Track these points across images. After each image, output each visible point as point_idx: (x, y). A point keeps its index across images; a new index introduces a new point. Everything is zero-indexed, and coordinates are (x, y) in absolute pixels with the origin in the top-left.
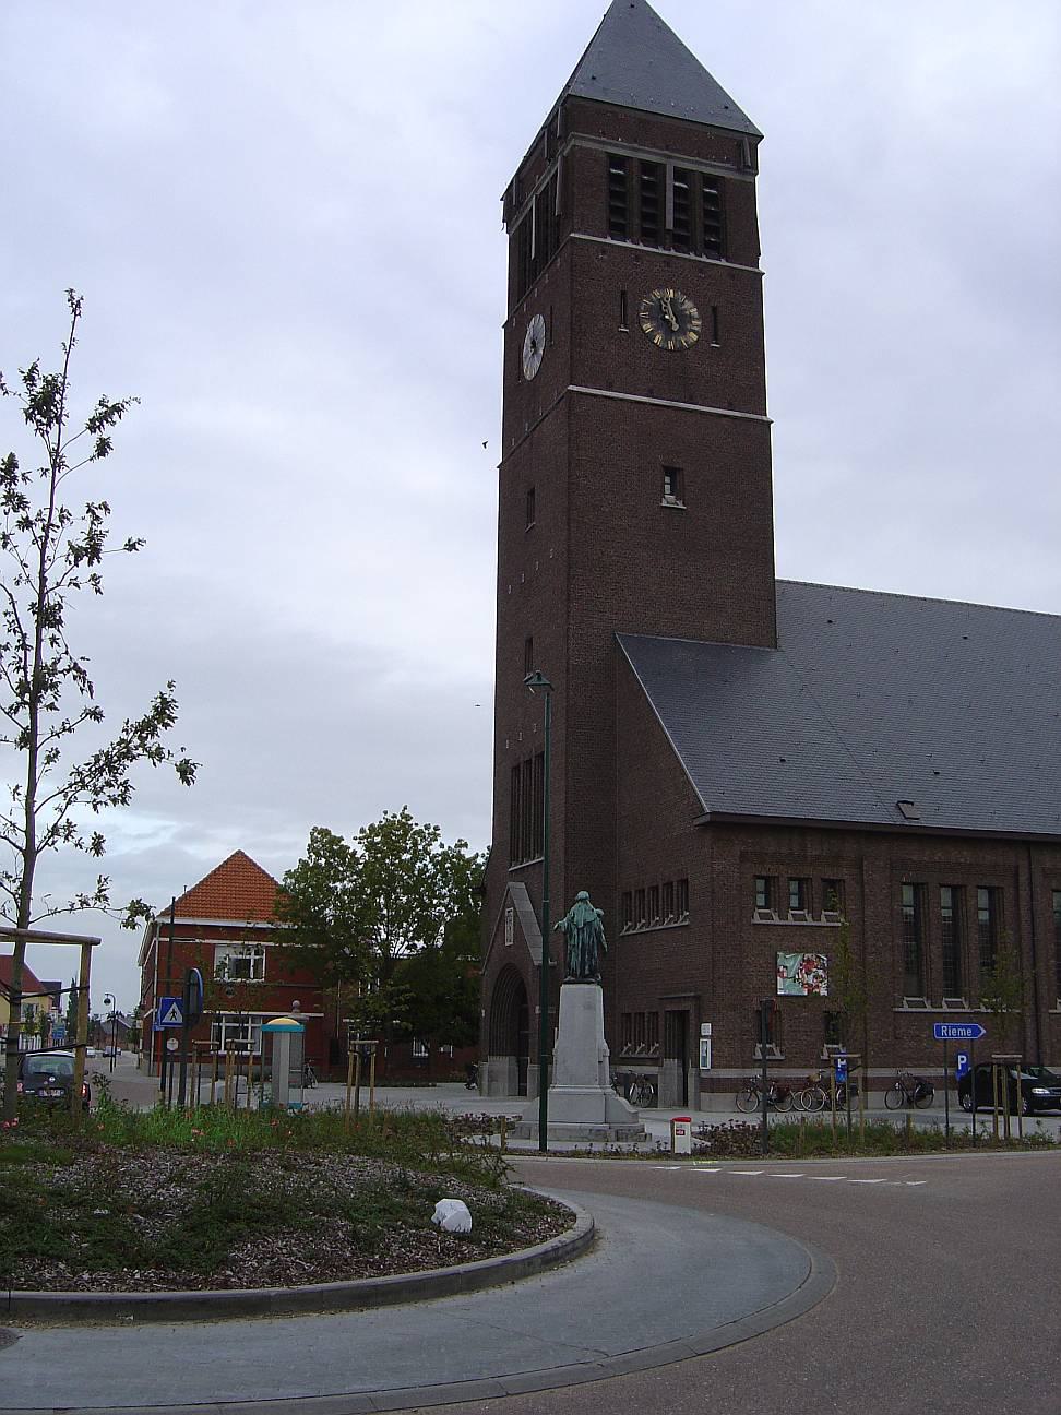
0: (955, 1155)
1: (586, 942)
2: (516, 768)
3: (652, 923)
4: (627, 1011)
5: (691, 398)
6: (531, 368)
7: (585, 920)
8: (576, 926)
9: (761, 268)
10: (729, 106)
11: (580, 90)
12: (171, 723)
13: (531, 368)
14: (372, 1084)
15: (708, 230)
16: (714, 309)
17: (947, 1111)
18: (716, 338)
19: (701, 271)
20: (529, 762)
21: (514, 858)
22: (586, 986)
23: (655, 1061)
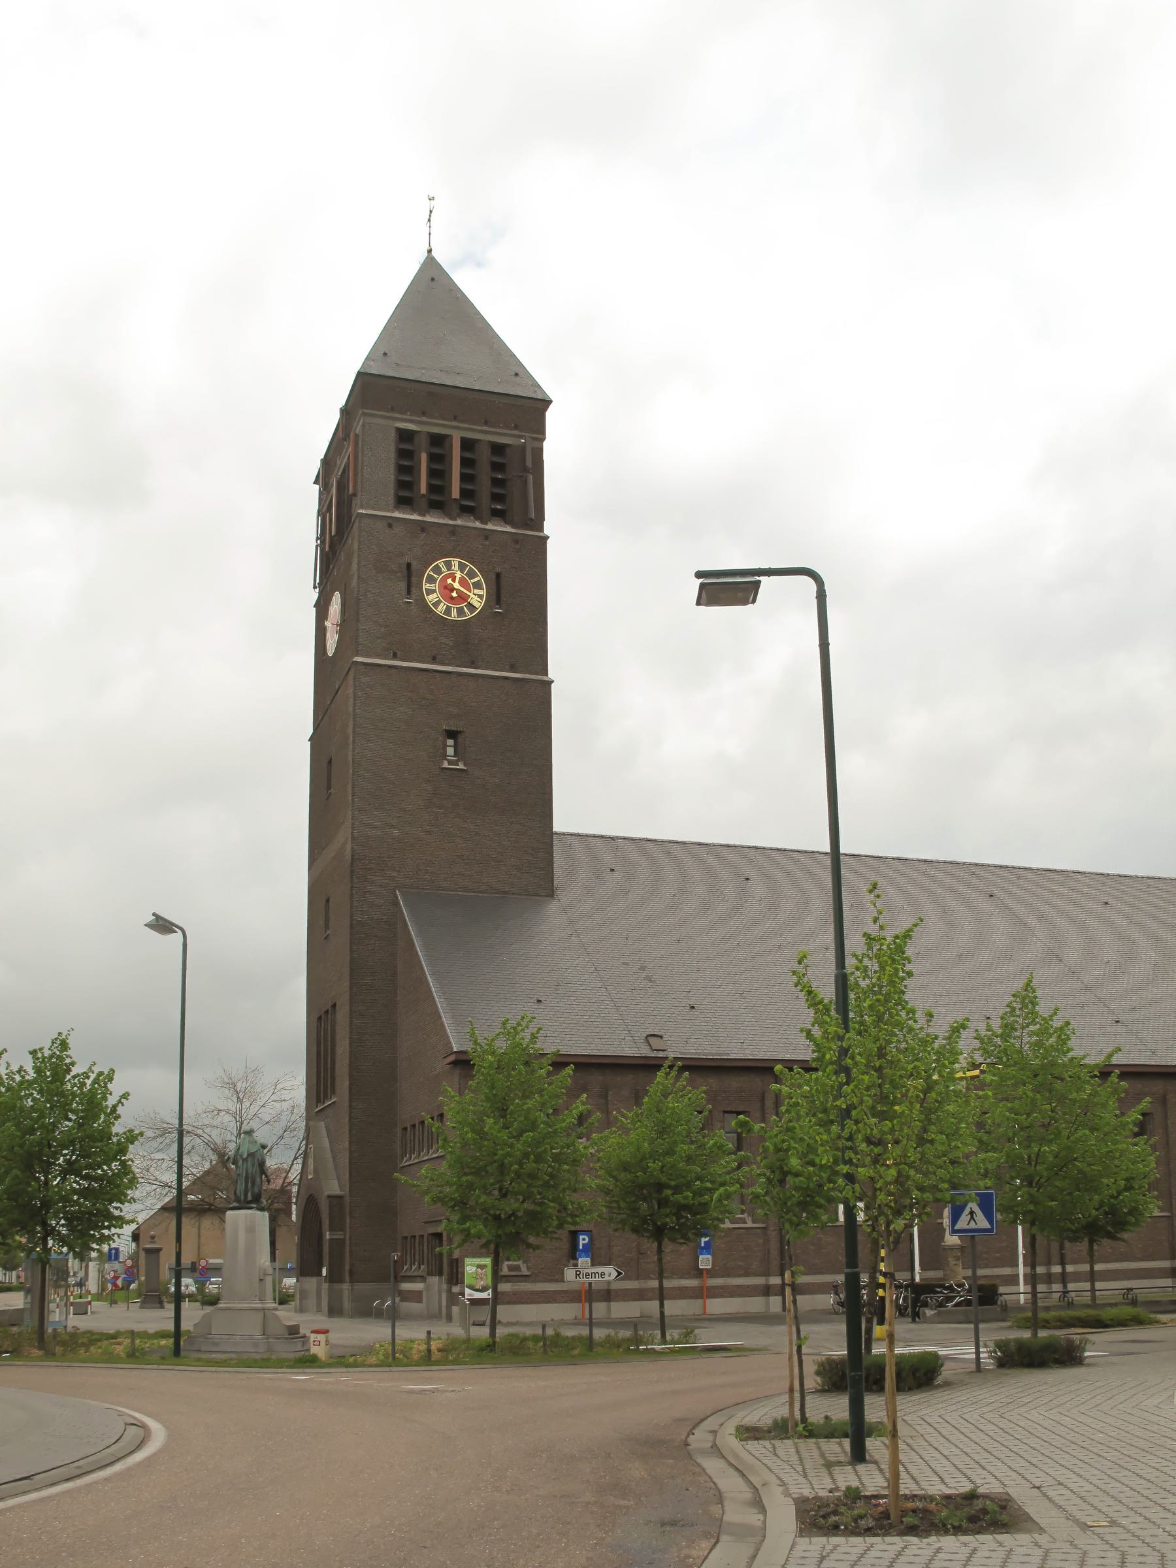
0: (918, 1349)
1: (250, 1171)
2: (320, 1018)
3: (422, 1154)
4: (405, 1235)
5: (473, 663)
6: (331, 649)
7: (248, 1151)
8: (241, 1156)
9: (547, 531)
10: (519, 372)
11: (363, 371)
12: (533, 1028)
13: (331, 649)
14: (583, 1300)
15: (496, 498)
16: (498, 576)
17: (662, 1314)
18: (498, 601)
19: (486, 538)
20: (327, 1012)
21: (318, 1101)
22: (249, 1211)
23: (422, 1278)
